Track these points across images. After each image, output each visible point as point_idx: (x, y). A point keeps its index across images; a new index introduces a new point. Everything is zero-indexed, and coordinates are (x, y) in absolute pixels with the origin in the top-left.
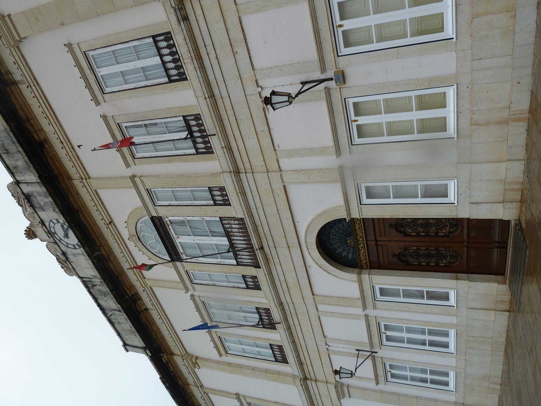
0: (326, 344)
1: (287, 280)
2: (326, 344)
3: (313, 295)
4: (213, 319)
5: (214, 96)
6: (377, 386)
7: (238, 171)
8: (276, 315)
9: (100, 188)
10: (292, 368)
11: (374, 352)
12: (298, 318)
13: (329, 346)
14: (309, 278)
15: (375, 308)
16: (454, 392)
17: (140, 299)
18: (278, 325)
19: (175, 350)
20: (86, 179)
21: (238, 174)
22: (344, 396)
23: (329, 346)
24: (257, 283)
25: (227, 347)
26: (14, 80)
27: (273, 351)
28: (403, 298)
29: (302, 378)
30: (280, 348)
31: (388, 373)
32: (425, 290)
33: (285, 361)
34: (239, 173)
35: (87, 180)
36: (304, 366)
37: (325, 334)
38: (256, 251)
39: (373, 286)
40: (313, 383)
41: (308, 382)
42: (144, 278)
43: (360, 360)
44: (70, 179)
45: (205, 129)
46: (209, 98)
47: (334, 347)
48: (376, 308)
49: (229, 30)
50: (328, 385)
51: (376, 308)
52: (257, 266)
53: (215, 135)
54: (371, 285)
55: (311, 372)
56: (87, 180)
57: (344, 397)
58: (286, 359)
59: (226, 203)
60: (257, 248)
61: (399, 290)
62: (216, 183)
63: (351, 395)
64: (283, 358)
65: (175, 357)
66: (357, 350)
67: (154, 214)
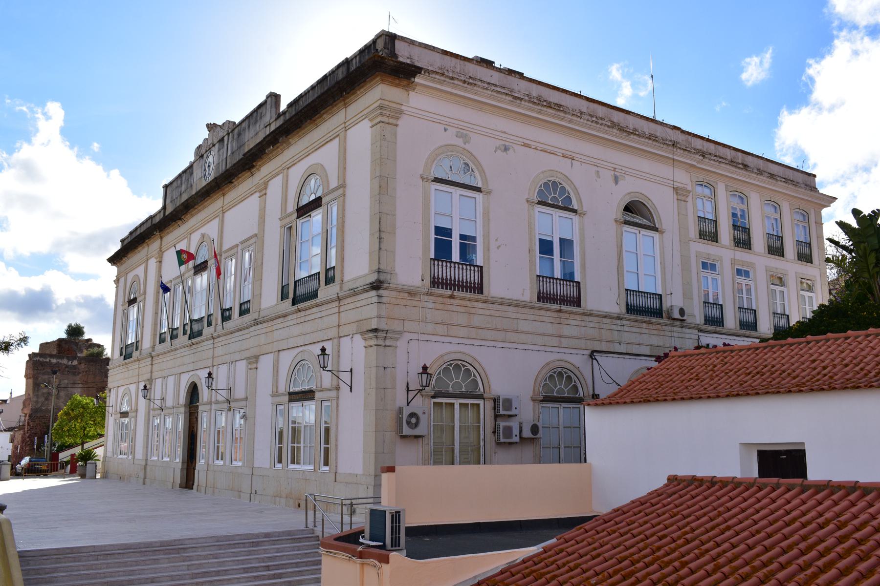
3: (279, 351)
44: (346, 106)
47: (232, 367)
66: (351, 369)
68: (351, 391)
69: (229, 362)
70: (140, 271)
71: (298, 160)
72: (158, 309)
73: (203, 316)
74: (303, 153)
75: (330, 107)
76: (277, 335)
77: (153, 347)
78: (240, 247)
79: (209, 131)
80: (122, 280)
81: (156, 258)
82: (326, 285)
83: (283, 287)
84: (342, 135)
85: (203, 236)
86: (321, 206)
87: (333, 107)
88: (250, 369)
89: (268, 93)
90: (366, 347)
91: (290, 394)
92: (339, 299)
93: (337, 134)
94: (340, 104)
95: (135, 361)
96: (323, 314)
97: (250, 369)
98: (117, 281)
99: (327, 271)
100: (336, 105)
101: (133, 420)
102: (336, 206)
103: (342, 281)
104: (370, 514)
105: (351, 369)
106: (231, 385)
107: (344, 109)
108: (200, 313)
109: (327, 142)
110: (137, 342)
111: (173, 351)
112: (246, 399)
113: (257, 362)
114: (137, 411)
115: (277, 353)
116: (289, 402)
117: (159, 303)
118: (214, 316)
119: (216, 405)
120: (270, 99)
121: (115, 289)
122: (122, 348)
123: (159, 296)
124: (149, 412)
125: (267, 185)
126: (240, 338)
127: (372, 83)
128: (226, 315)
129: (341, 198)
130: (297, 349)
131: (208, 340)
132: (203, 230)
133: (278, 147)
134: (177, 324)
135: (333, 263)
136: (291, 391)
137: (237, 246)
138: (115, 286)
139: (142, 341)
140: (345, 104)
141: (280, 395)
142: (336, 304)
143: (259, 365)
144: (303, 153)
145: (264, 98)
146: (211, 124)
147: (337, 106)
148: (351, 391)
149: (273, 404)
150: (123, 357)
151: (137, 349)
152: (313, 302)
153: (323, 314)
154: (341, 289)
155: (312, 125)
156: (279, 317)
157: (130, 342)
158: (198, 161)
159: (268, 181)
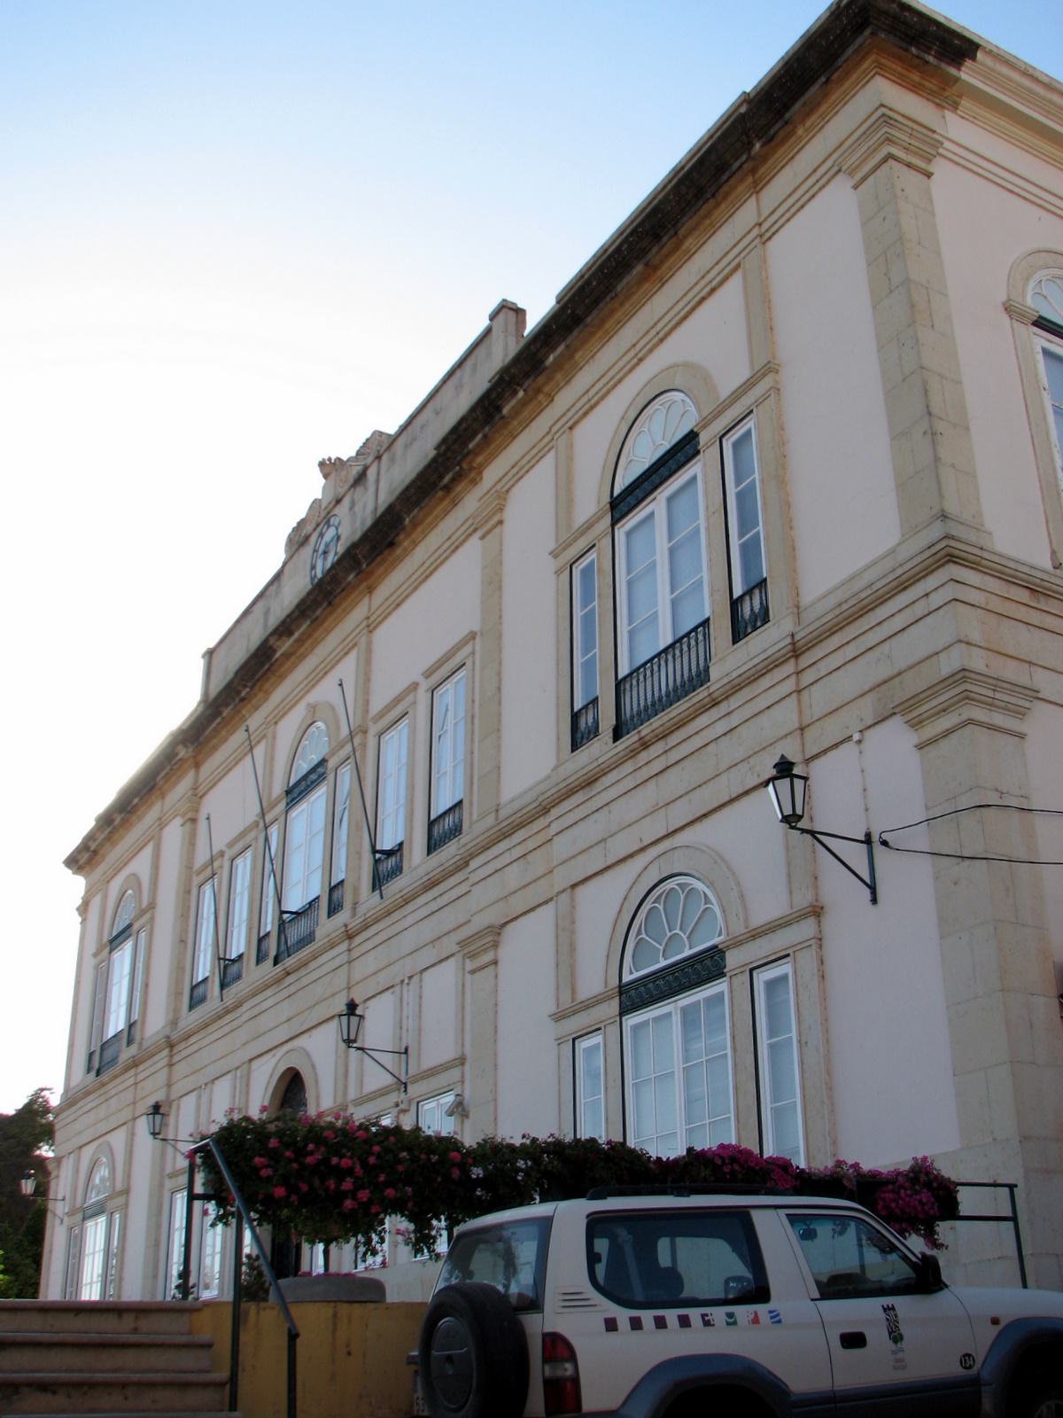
0: (206, 1084)
1: (669, 770)
2: (206, 1084)
3: (574, 886)
4: (727, 440)
5: (407, 903)
6: (549, 1018)
7: (798, 652)
8: (395, 887)
9: (744, 278)
10: (190, 1019)
11: (406, 1087)
12: (580, 824)
13: (408, 984)
14: (747, 793)
15: (560, 1041)
16: (414, 1260)
17: (454, 502)
18: (378, 896)
19: (208, 767)
20: (761, 236)
21: (791, 654)
22: (915, 724)
23: (408, 984)
24: (761, 621)
25: (445, 689)
26: (883, 76)
27: (672, 646)
28: (768, 1044)
29: (349, 927)
30: (457, 830)
31: (598, 1037)
32: (684, 1128)
33: (742, 630)
34: (797, 657)
35: (758, 239)
36: (184, 1043)
37: (216, 1082)
38: (636, 731)
39: (788, 955)
40: (790, 685)
41: (344, 946)
42: (571, 428)
43: (387, 1059)
44: (757, 188)
45: (748, 634)
46: (709, 695)
47: (410, 994)
48: (559, 1044)
49: (966, 636)
50: (346, 991)
51: (559, 1044)
52: (617, 734)
53: (382, 897)
54: (602, 1025)
55: (823, 668)
56: (758, 239)
57: (913, 726)
58: (592, 736)
59: (738, 634)
60: (643, 734)
61: (791, 1032)
62: (777, 598)
63: (932, 751)
64: (587, 731)
65: (192, 773)
66: (406, 1049)
67: (704, 438)
68: (874, 900)
69: (398, 980)
70: (141, 865)
71: (330, 665)
72: (186, 932)
73: (706, 616)
74: (621, 364)
75: (712, 202)
76: (562, 847)
77: (174, 1023)
78: (227, 856)
79: (326, 476)
80: (96, 903)
81: (183, 815)
82: (329, 916)
83: (575, 717)
84: (363, 641)
85: (313, 708)
86: (698, 452)
87: (718, 205)
88: (473, 972)
89: (493, 304)
90: (920, 747)
91: (623, 989)
92: (350, 937)
93: (736, 261)
94: (741, 188)
95: (127, 1069)
96: (735, 720)
97: (473, 972)
98: (83, 909)
99: (332, 890)
100: (725, 198)
101: (117, 1216)
102: (349, 771)
103: (798, 607)
104: (616, 1326)
105: (406, 1049)
106: (409, 1039)
107: (754, 198)
108: (116, 1027)
109: (703, 299)
110: (131, 1026)
111: (228, 1011)
112: (461, 1061)
113: (496, 945)
114: (126, 1192)
115: (564, 897)
116: (621, 1014)
117: (188, 917)
118: (348, 889)
119: (173, 1180)
120: (501, 317)
121: (77, 928)
122: (91, 1055)
123: (189, 900)
124: (161, 1185)
125: (505, 499)
126: (434, 906)
127: (847, 84)
128: (386, 864)
129: (471, 658)
130: (630, 863)
131: (332, 945)
132: (312, 697)
133: (539, 391)
134: (239, 944)
135: (135, 1017)
136: (627, 978)
137: (414, 686)
138: (80, 919)
139: (143, 1022)
140: (755, 184)
141: (587, 1005)
142: (789, 668)
143: (504, 952)
144: (621, 364)
145: (486, 322)
146: (330, 459)
147: (730, 199)
148: (874, 900)
149: (559, 1041)
150: (93, 1073)
151: (130, 1042)
152: (701, 694)
153: (735, 720)
154: (354, 914)
155: (647, 285)
156: (571, 792)
157: (111, 1033)
158: (351, 492)
159: (507, 491)
